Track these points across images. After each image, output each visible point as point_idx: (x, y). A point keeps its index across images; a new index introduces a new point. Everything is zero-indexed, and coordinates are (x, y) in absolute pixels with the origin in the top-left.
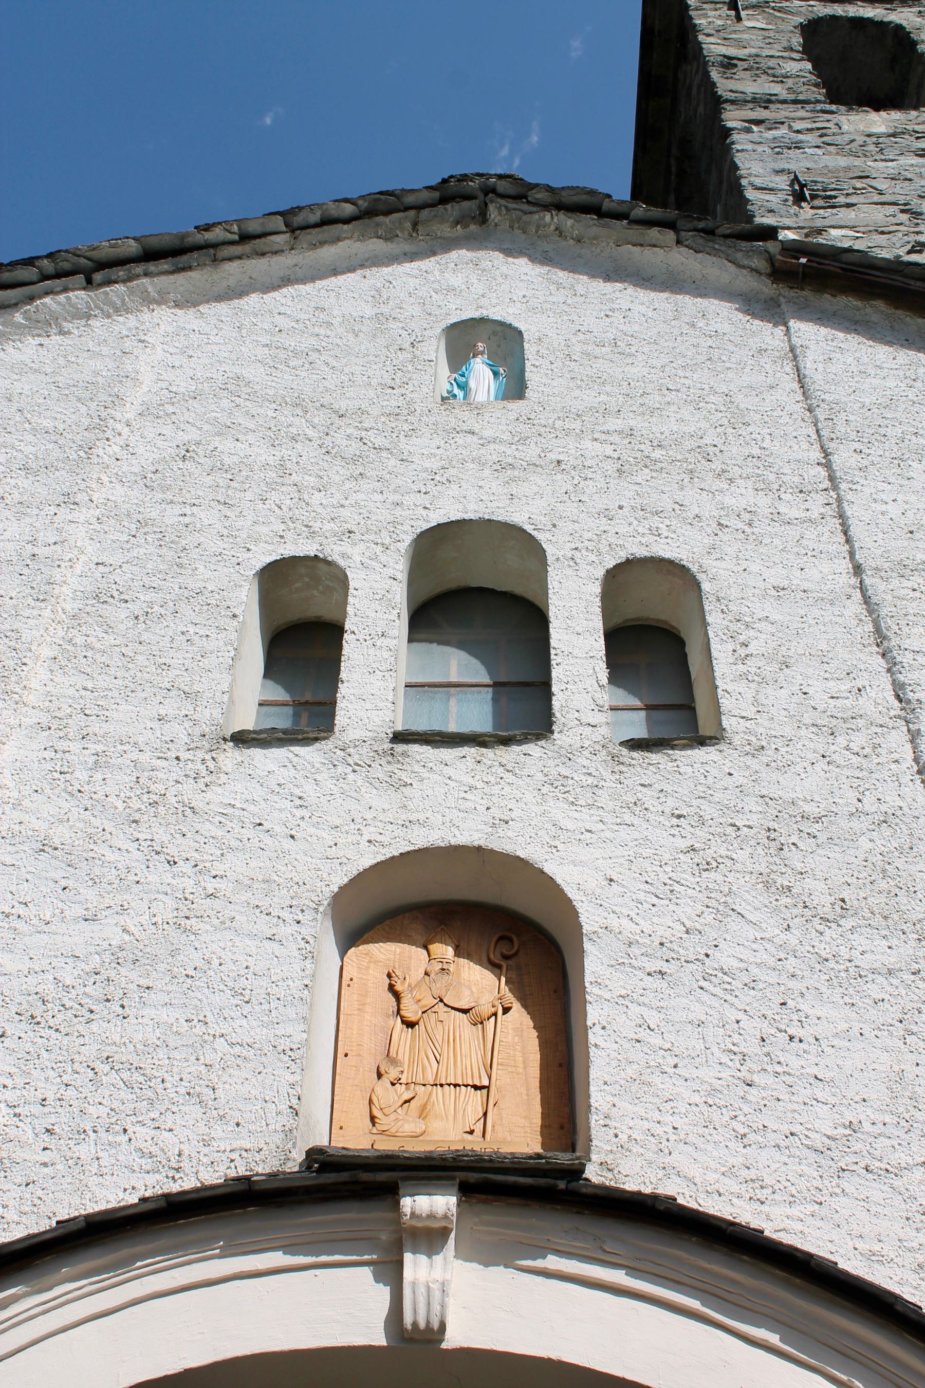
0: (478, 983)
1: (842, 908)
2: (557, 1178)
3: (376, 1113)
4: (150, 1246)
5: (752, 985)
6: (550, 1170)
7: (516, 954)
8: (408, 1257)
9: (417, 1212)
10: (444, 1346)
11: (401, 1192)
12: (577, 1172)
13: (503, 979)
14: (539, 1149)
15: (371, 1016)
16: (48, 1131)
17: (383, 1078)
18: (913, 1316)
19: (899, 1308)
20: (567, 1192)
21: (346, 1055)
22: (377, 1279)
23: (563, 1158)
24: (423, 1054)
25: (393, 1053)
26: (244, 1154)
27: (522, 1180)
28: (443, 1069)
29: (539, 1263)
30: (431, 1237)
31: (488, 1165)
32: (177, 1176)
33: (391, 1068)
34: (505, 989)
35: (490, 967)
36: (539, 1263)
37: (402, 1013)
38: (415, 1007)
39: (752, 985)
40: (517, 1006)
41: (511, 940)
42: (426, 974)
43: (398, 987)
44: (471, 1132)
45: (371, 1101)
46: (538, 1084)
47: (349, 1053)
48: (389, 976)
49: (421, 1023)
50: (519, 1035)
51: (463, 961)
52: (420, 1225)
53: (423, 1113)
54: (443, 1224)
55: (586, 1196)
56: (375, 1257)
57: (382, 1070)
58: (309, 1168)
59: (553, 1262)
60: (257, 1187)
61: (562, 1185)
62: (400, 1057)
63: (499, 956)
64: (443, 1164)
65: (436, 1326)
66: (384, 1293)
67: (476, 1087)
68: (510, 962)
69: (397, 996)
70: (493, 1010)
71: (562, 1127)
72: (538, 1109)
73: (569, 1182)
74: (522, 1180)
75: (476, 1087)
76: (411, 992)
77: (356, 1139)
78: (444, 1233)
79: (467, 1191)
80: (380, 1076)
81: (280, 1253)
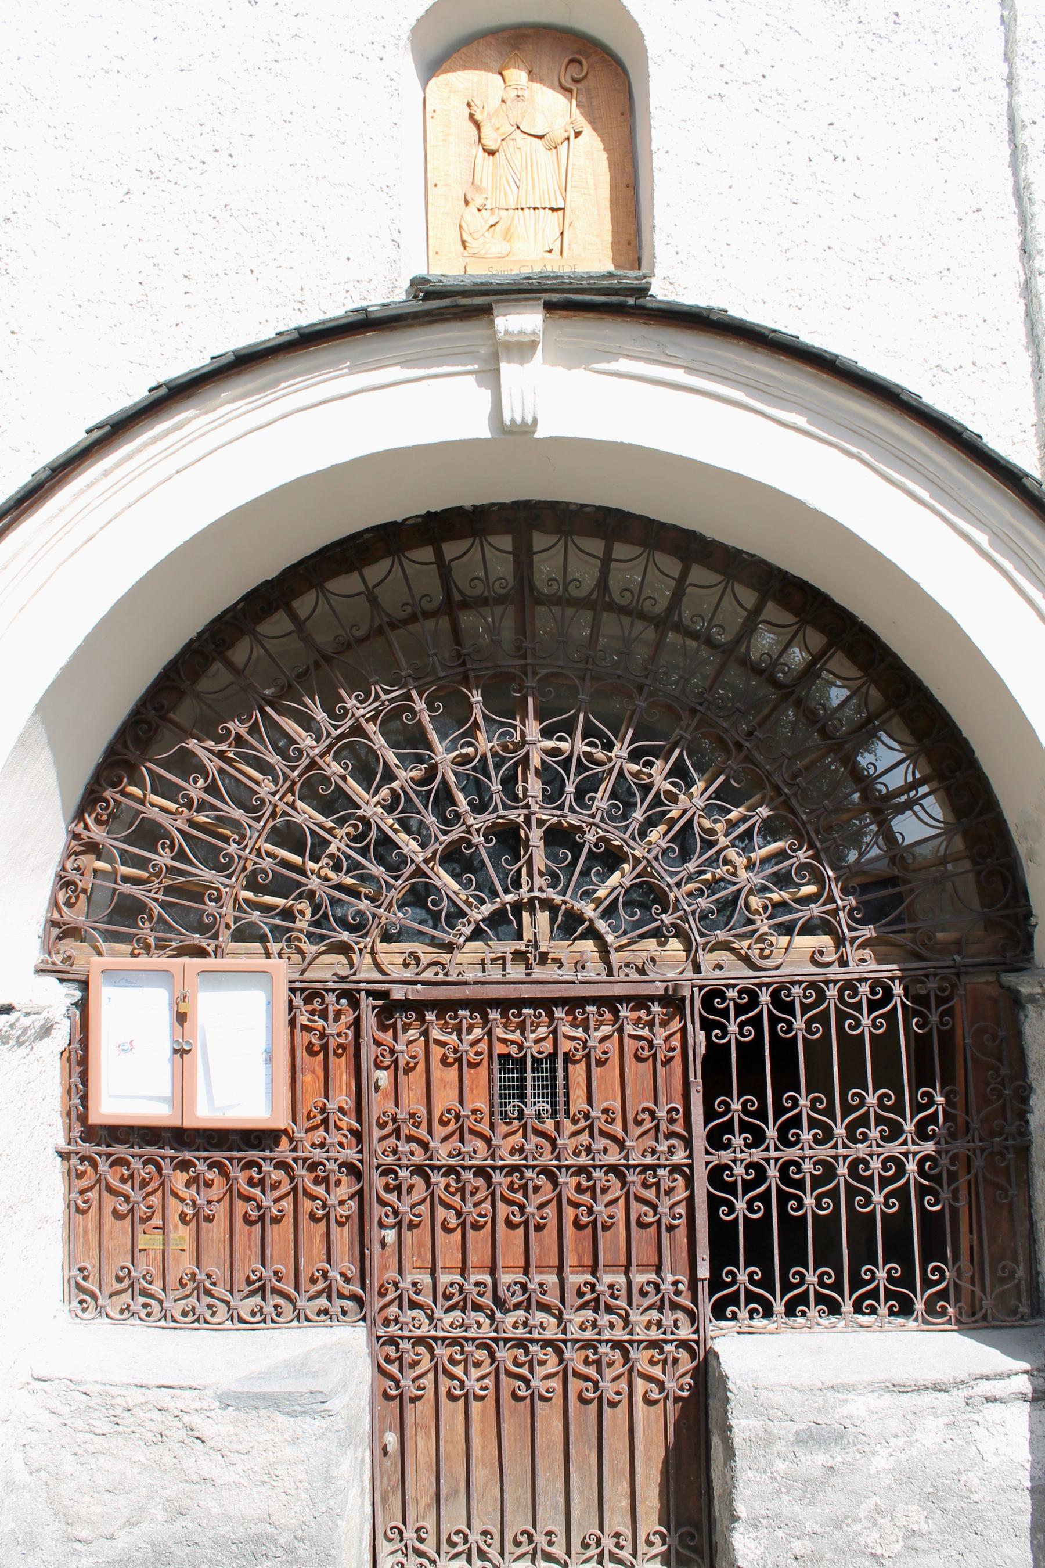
0: (551, 107)
1: (895, 23)
2: (627, 296)
3: (466, 237)
4: (290, 371)
5: (804, 105)
6: (620, 289)
7: (585, 77)
8: (504, 366)
9: (510, 330)
10: (536, 436)
11: (495, 313)
12: (643, 291)
13: (574, 102)
14: (610, 267)
15: (454, 146)
16: (186, 277)
17: (470, 205)
18: (914, 403)
19: (904, 397)
20: (636, 307)
21: (436, 185)
22: (480, 384)
23: (630, 277)
24: (504, 180)
25: (477, 181)
26: (357, 285)
27: (672, 1489)
28: (523, 193)
29: (613, 366)
30: (523, 349)
31: (568, 287)
32: (302, 308)
33: (477, 195)
34: (576, 112)
35: (562, 91)
36: (613, 366)
37: (483, 141)
38: (494, 135)
39: (804, 105)
40: (588, 131)
41: (581, 63)
42: (503, 101)
43: (478, 117)
44: (550, 251)
45: (461, 227)
46: (608, 204)
47: (439, 183)
48: (469, 105)
49: (501, 150)
50: (590, 157)
51: (537, 86)
52: (513, 340)
53: (507, 236)
54: (532, 338)
55: (652, 309)
56: (476, 367)
57: (469, 199)
58: (415, 297)
59: (624, 365)
60: (373, 316)
61: (631, 301)
62: (484, 184)
63: (570, 81)
64: (530, 287)
65: (530, 421)
66: (485, 396)
67: (553, 210)
68: (579, 86)
69: (477, 125)
70: (566, 135)
71: (629, 244)
72: (608, 227)
73: (637, 298)
74: (672, 1489)
75: (553, 210)
76: (490, 120)
77: (450, 267)
78: (533, 345)
79: (550, 307)
80: (467, 203)
81: (398, 368)
